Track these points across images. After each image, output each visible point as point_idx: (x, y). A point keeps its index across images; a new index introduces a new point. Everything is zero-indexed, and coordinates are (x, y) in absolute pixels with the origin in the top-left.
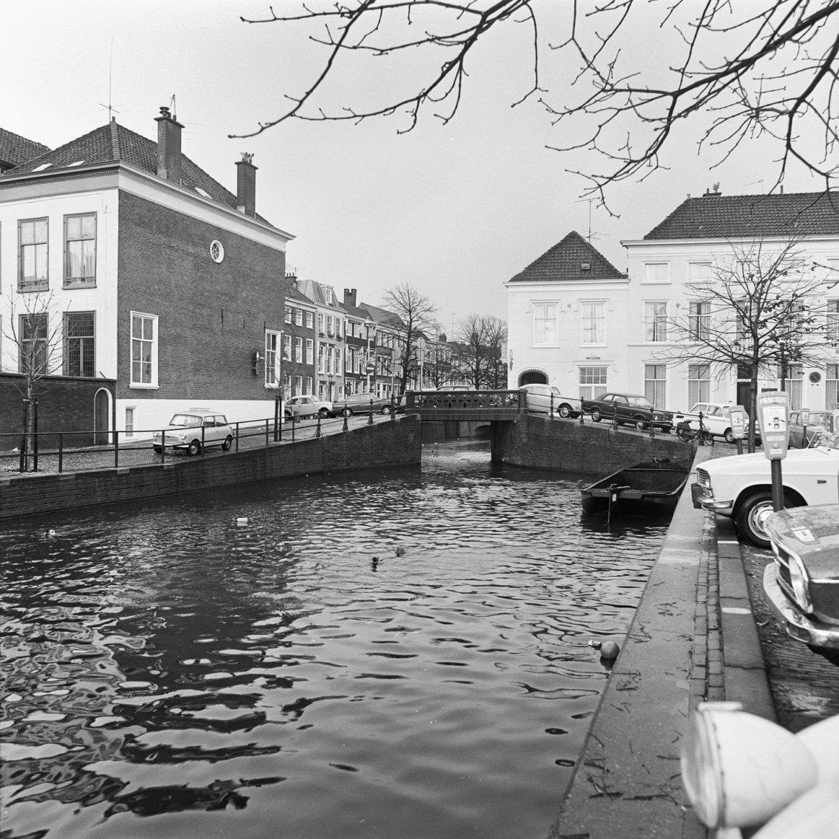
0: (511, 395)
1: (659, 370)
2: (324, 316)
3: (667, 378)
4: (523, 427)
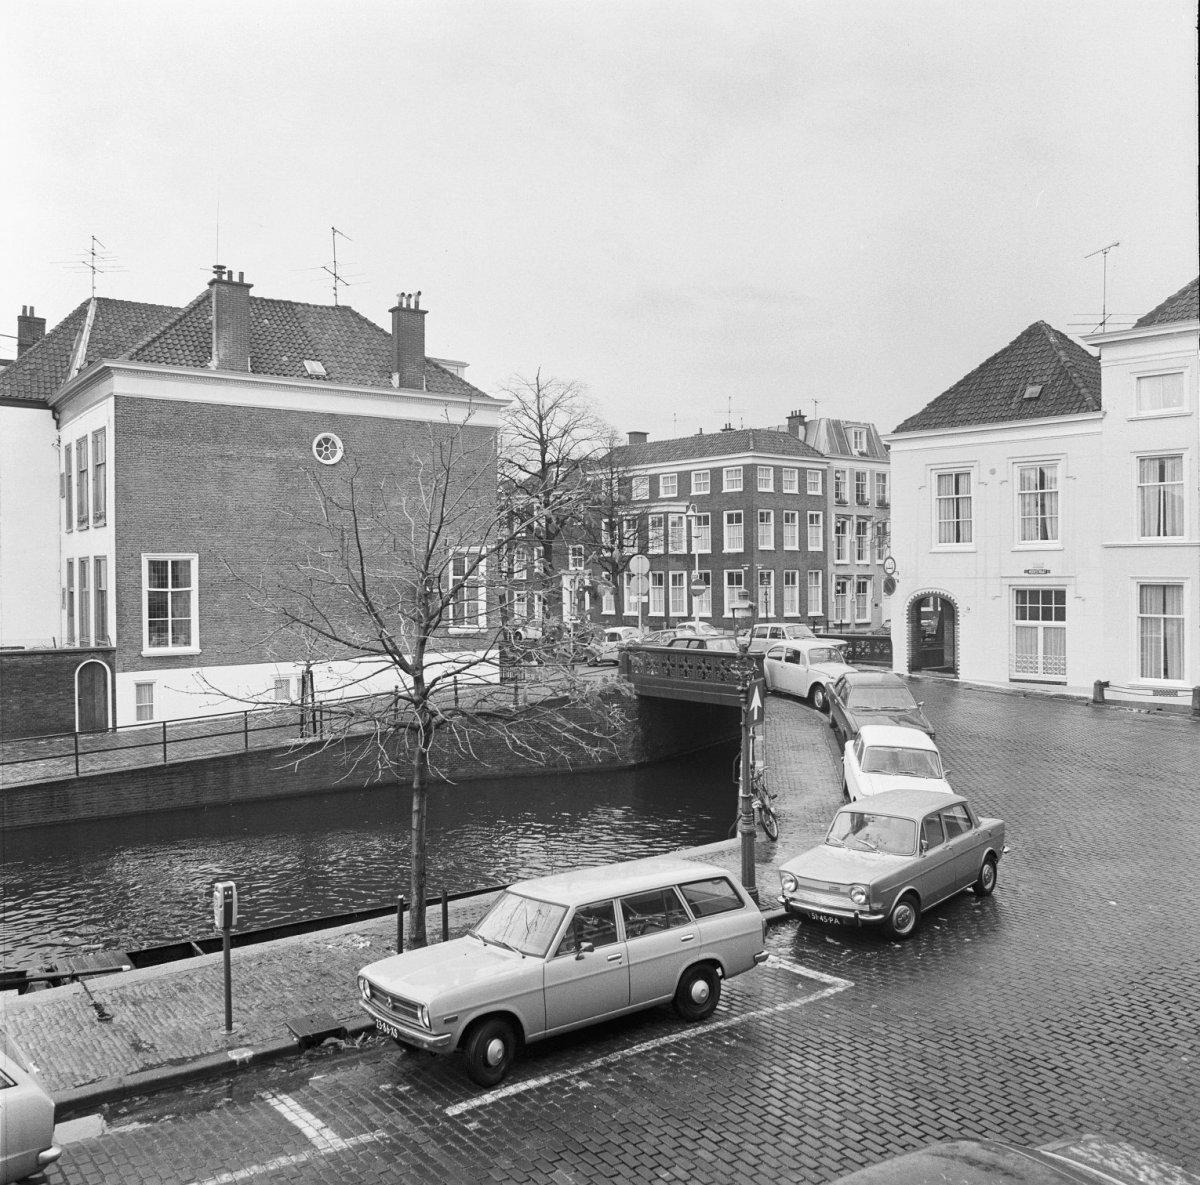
0: (863, 642)
2: (847, 473)
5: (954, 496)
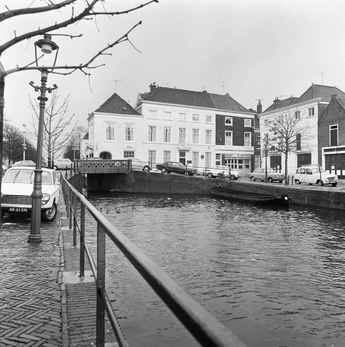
1: (153, 153)
3: (157, 156)
4: (132, 176)
5: (151, 131)
